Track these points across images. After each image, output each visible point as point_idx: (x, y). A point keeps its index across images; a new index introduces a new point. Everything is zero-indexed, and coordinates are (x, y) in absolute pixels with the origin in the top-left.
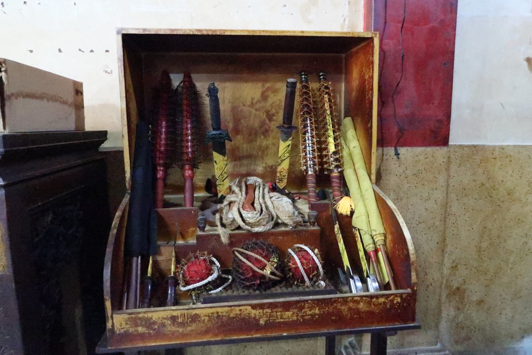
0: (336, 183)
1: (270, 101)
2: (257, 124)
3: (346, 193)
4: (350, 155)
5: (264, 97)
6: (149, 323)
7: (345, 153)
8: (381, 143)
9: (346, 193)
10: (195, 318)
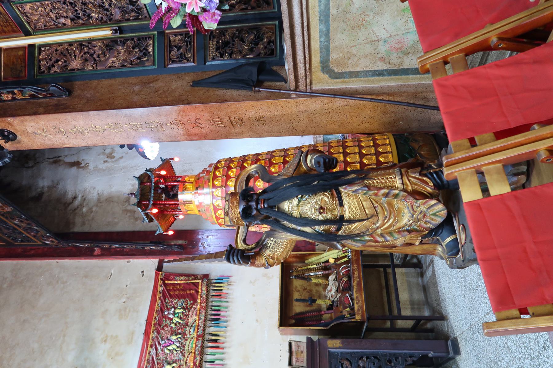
0: (326, 264)
1: (300, 289)
2: (308, 294)
3: (327, 261)
4: (317, 260)
5: (298, 291)
6: (358, 310)
7: (316, 262)
8: (314, 250)
9: (327, 261)
10: (357, 298)
